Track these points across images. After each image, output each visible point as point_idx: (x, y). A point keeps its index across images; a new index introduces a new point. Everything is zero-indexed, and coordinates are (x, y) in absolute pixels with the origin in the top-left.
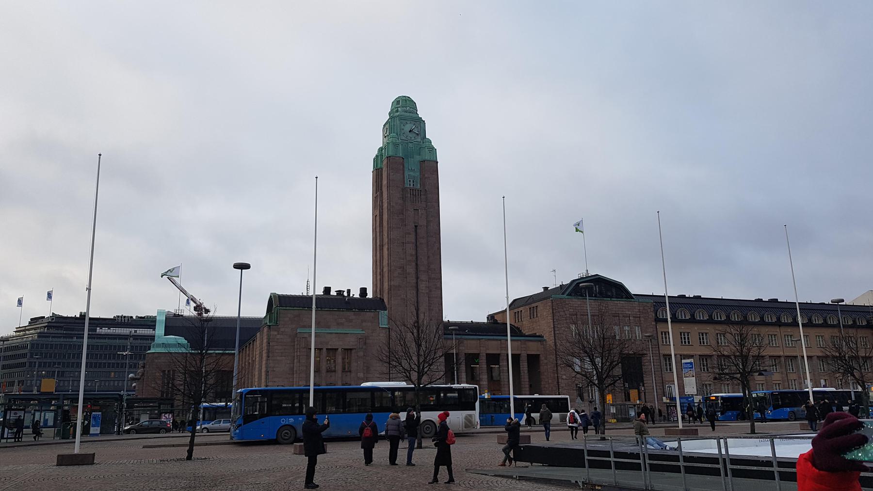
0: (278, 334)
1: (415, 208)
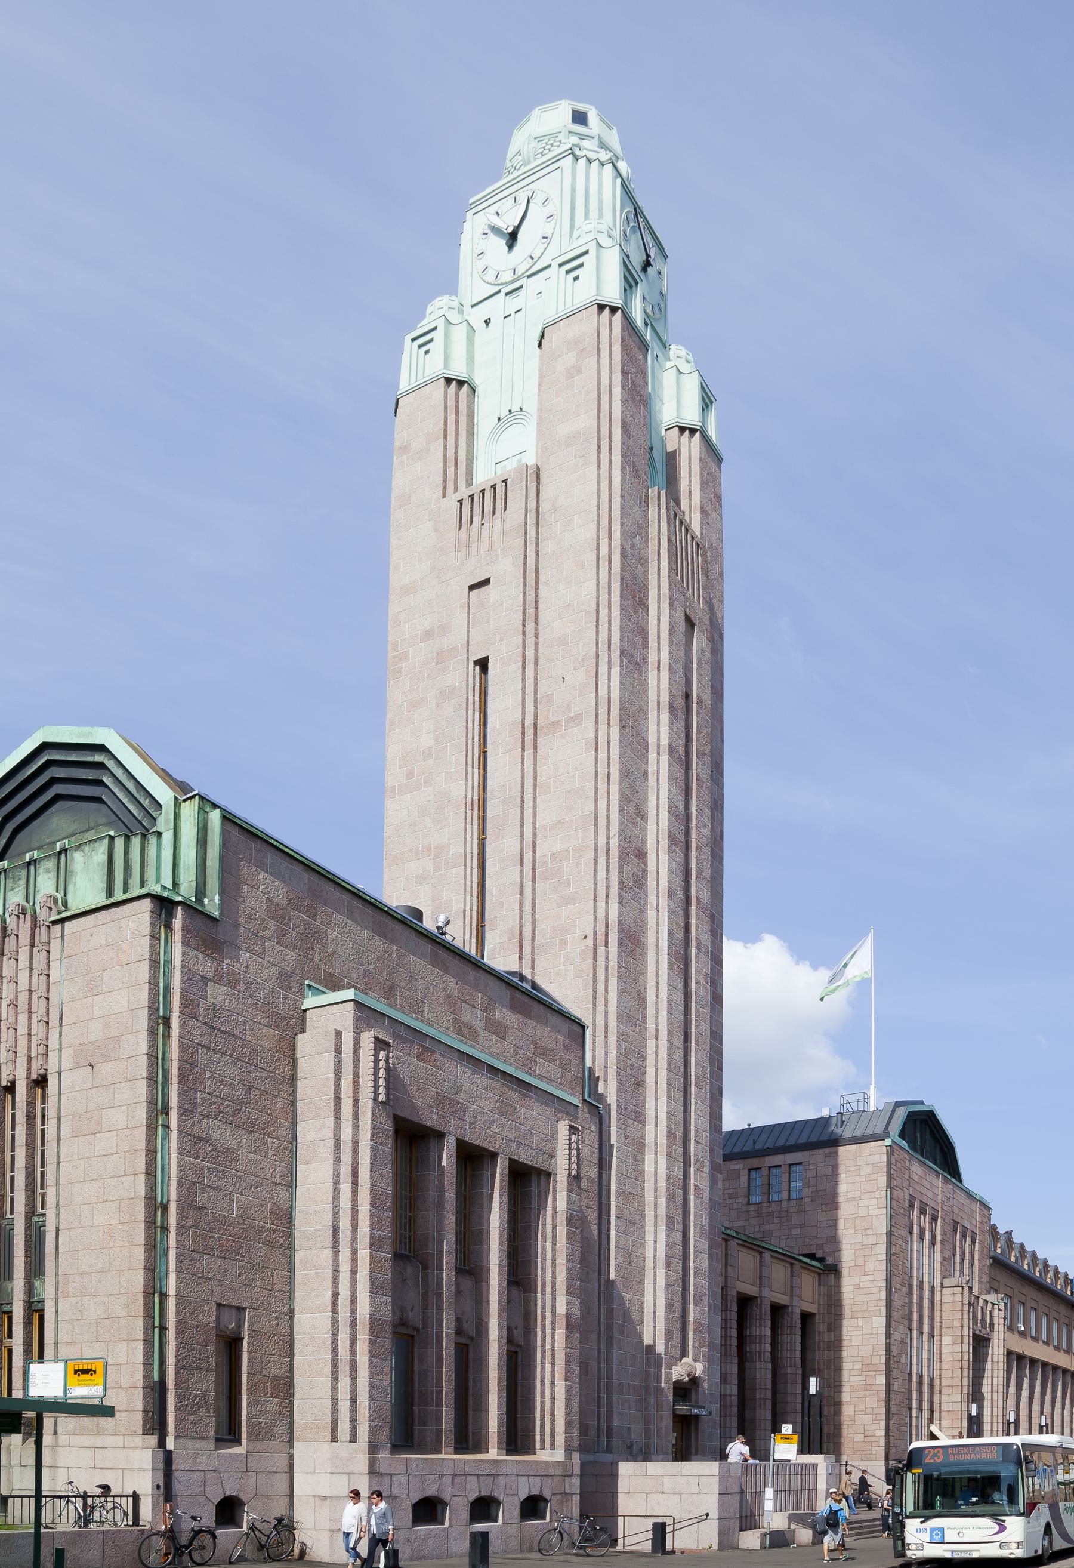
0: (218, 979)
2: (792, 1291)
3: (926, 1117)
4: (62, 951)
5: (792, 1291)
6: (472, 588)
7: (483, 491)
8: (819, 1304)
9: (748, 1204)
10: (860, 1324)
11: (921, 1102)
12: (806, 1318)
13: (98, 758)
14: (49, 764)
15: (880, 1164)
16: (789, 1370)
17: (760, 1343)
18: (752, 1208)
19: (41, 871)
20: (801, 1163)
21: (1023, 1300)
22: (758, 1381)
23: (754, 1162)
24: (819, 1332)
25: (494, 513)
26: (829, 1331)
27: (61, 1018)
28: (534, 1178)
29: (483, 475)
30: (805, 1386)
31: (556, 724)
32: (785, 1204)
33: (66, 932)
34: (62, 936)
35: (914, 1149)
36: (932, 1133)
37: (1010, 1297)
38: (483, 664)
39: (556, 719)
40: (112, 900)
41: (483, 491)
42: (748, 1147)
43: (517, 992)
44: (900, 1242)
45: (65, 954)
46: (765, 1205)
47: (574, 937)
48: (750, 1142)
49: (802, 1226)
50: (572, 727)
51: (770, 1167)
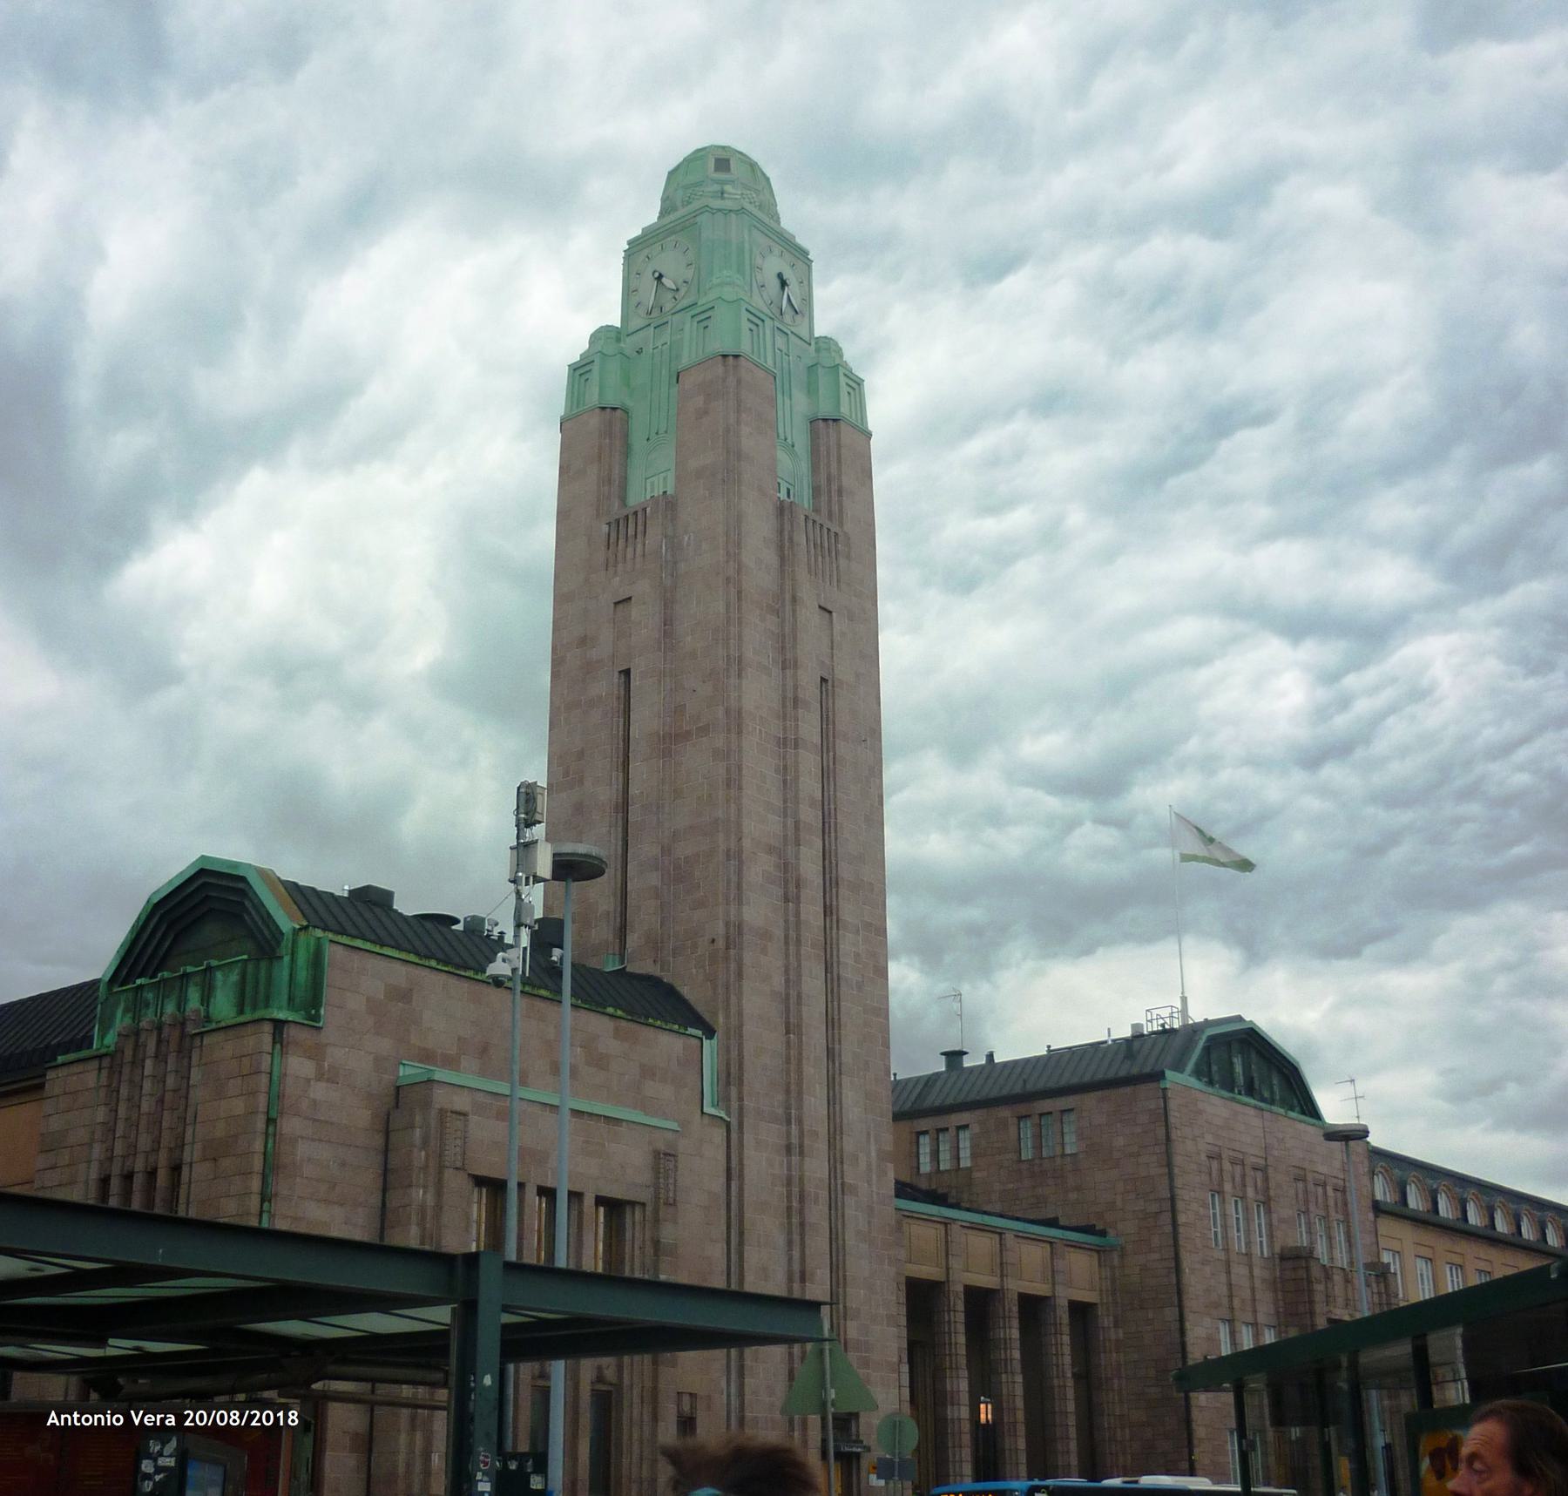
0: (320, 1077)
1: (823, 605)
2: (1053, 1277)
3: (1244, 1036)
4: (201, 1059)
5: (1053, 1277)
6: (616, 604)
7: (636, 513)
8: (1101, 1291)
9: (1020, 1161)
10: (1151, 1315)
11: (1239, 1019)
12: (1081, 1311)
13: (241, 885)
14: (205, 885)
15: (1157, 1111)
16: (1056, 1382)
17: (1005, 1349)
18: (1024, 1166)
19: (191, 984)
20: (1072, 1110)
21: (1457, 1260)
22: (1004, 1398)
23: (1022, 1109)
24: (1103, 1328)
25: (636, 538)
26: (1116, 1326)
27: (195, 1117)
28: (628, 1210)
29: (636, 497)
30: (975, 1412)
31: (689, 733)
32: (1059, 1161)
33: (205, 1042)
34: (201, 1046)
35: (1211, 1083)
36: (1259, 1053)
37: (1430, 1260)
38: (627, 673)
39: (688, 728)
40: (241, 1019)
41: (636, 513)
42: (1018, 1089)
43: (622, 1021)
44: (1194, 1206)
45: (203, 1061)
46: (1037, 1161)
47: (704, 941)
48: (1021, 1082)
49: (1078, 1189)
50: (702, 737)
51: (1041, 1115)
